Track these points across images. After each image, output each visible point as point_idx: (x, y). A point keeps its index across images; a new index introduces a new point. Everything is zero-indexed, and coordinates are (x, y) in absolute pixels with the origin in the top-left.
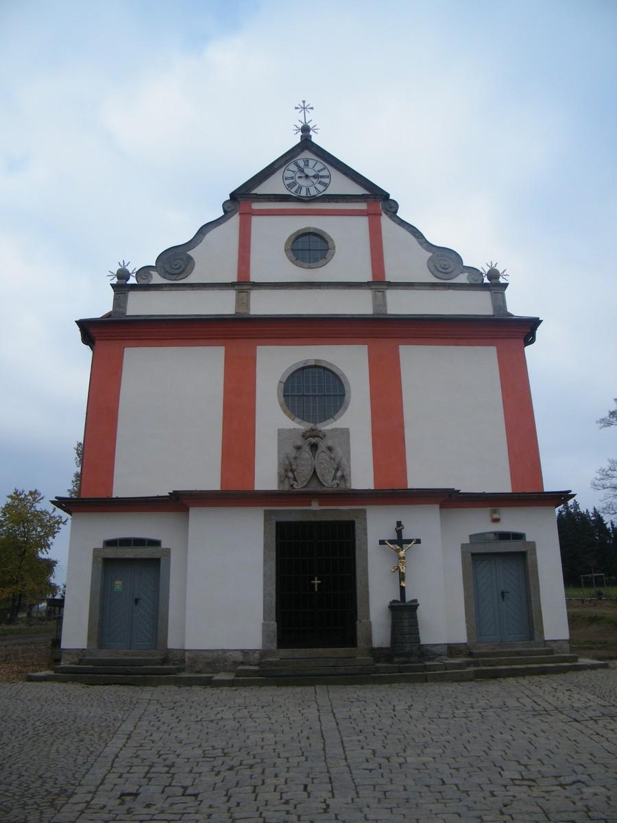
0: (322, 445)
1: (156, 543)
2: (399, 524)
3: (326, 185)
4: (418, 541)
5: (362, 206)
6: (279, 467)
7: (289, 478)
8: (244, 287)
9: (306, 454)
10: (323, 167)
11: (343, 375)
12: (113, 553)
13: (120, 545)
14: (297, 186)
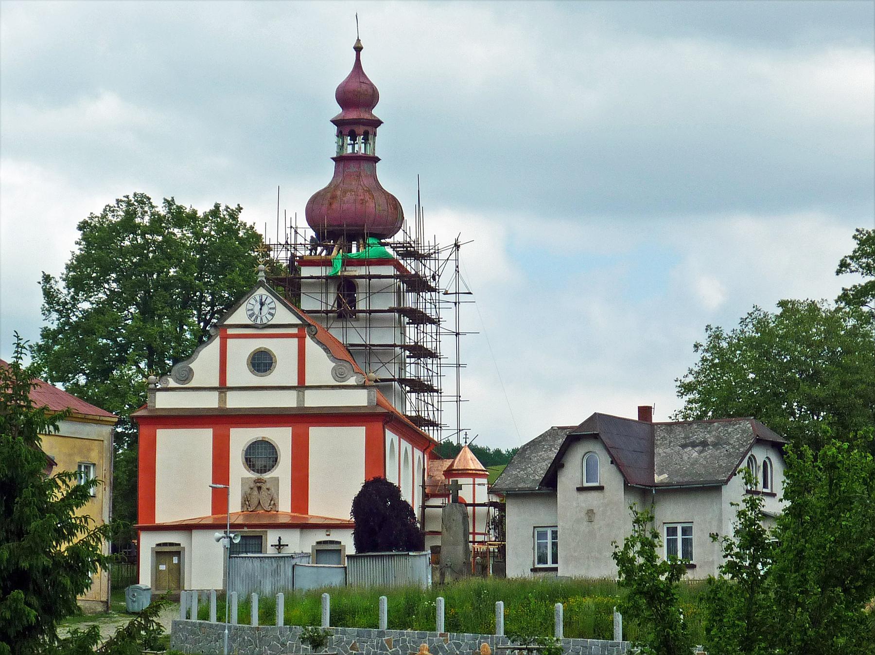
0: (264, 487)
1: (179, 545)
2: (280, 538)
3: (273, 315)
4: (287, 545)
5: (295, 331)
7: (246, 504)
9: (255, 492)
10: (271, 300)
12: (160, 549)
13: (163, 546)
14: (254, 316)
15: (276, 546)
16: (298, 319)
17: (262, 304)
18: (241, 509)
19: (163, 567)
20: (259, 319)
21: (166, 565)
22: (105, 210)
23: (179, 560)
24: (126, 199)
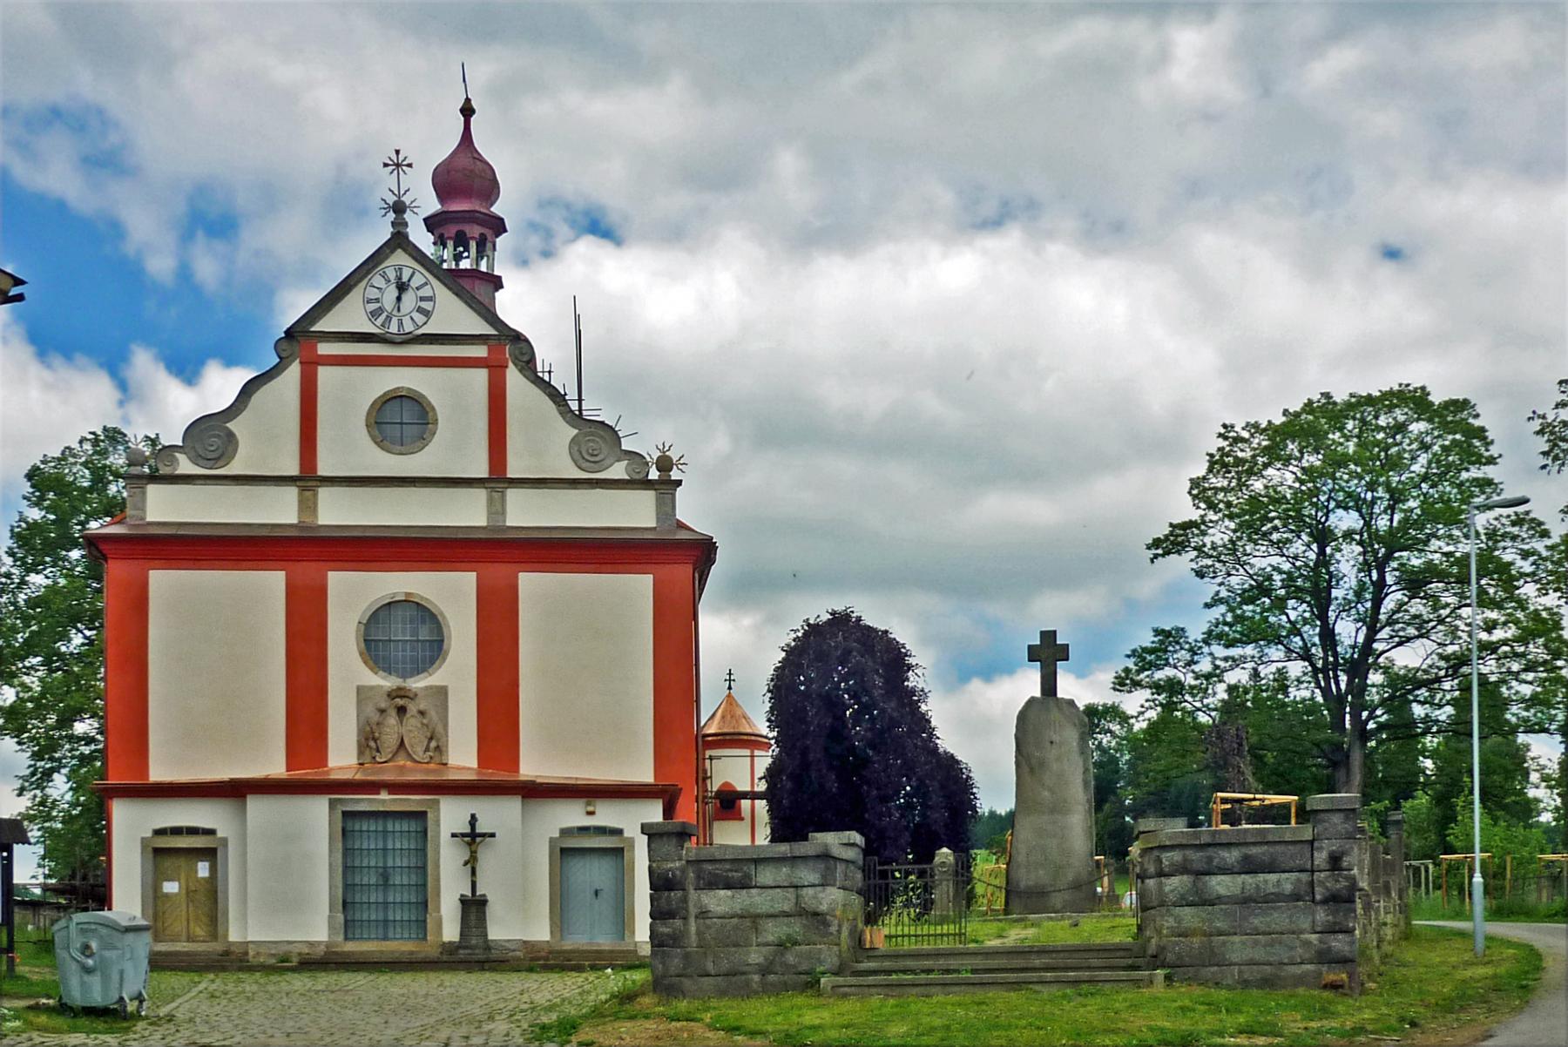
0: (412, 708)
1: (211, 832)
2: (473, 817)
3: (427, 314)
5: (480, 351)
6: (358, 735)
7: (371, 748)
8: (310, 484)
9: (392, 720)
10: (424, 280)
11: (442, 613)
13: (171, 834)
15: (463, 835)
16: (488, 326)
17: (402, 287)
18: (358, 759)
19: (171, 887)
20: (395, 321)
21: (179, 880)
22: (63, 453)
23: (213, 869)
24: (92, 436)
